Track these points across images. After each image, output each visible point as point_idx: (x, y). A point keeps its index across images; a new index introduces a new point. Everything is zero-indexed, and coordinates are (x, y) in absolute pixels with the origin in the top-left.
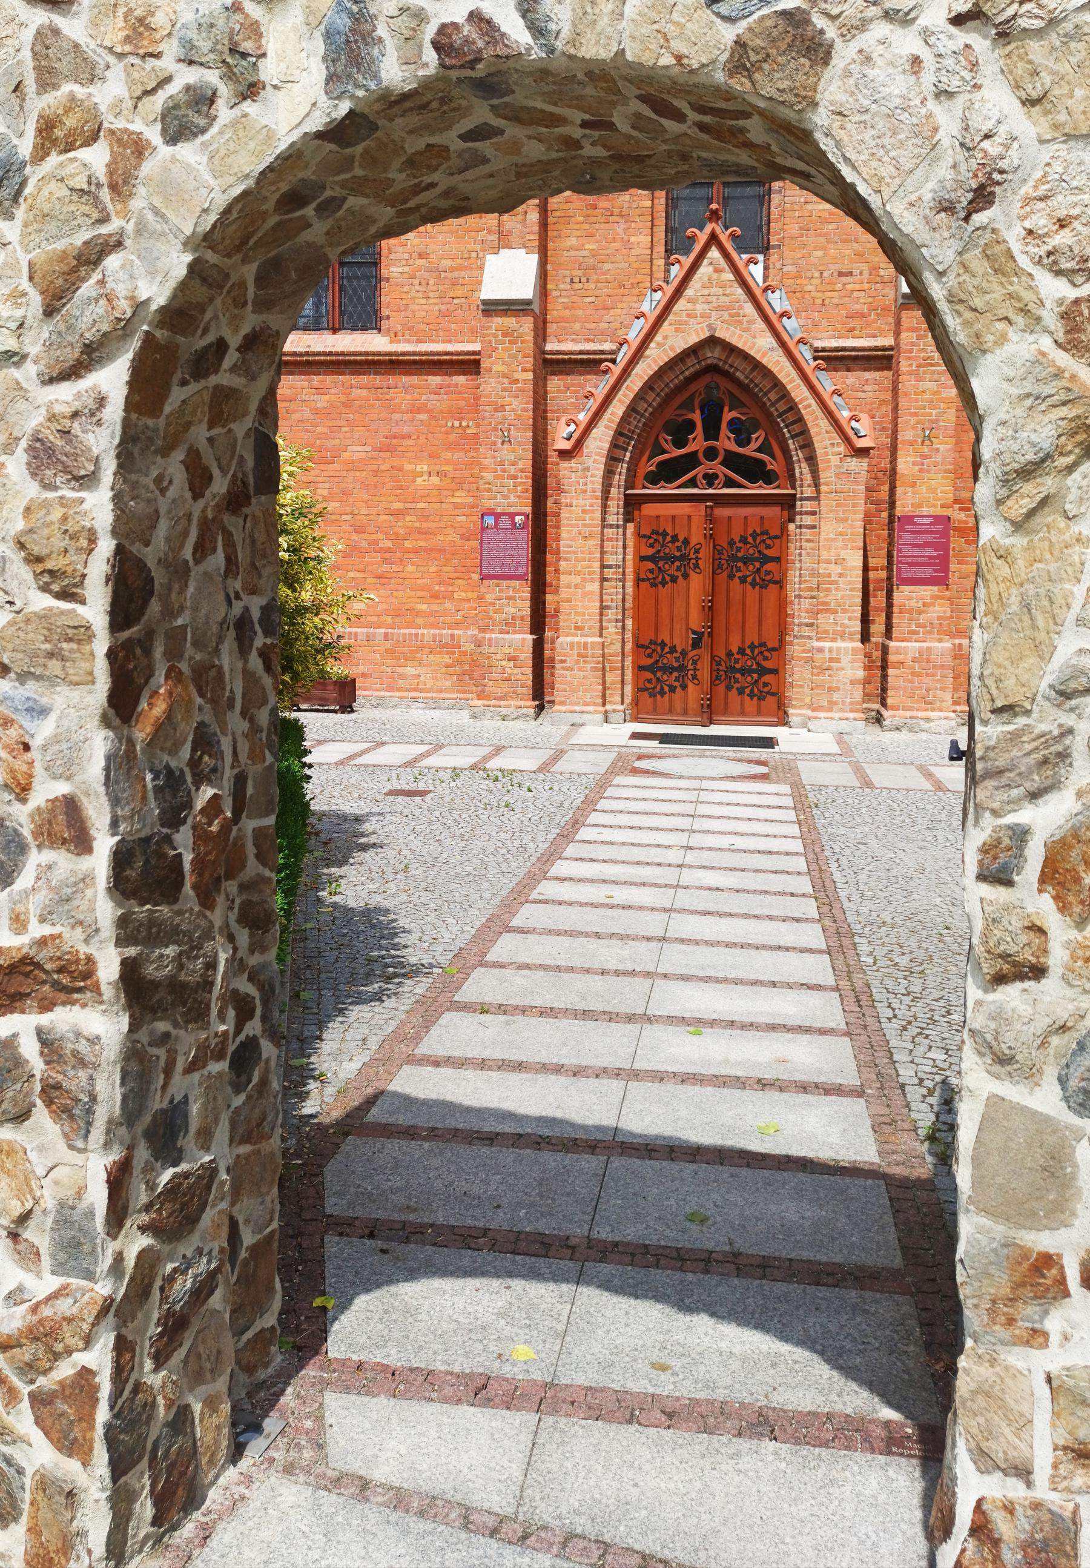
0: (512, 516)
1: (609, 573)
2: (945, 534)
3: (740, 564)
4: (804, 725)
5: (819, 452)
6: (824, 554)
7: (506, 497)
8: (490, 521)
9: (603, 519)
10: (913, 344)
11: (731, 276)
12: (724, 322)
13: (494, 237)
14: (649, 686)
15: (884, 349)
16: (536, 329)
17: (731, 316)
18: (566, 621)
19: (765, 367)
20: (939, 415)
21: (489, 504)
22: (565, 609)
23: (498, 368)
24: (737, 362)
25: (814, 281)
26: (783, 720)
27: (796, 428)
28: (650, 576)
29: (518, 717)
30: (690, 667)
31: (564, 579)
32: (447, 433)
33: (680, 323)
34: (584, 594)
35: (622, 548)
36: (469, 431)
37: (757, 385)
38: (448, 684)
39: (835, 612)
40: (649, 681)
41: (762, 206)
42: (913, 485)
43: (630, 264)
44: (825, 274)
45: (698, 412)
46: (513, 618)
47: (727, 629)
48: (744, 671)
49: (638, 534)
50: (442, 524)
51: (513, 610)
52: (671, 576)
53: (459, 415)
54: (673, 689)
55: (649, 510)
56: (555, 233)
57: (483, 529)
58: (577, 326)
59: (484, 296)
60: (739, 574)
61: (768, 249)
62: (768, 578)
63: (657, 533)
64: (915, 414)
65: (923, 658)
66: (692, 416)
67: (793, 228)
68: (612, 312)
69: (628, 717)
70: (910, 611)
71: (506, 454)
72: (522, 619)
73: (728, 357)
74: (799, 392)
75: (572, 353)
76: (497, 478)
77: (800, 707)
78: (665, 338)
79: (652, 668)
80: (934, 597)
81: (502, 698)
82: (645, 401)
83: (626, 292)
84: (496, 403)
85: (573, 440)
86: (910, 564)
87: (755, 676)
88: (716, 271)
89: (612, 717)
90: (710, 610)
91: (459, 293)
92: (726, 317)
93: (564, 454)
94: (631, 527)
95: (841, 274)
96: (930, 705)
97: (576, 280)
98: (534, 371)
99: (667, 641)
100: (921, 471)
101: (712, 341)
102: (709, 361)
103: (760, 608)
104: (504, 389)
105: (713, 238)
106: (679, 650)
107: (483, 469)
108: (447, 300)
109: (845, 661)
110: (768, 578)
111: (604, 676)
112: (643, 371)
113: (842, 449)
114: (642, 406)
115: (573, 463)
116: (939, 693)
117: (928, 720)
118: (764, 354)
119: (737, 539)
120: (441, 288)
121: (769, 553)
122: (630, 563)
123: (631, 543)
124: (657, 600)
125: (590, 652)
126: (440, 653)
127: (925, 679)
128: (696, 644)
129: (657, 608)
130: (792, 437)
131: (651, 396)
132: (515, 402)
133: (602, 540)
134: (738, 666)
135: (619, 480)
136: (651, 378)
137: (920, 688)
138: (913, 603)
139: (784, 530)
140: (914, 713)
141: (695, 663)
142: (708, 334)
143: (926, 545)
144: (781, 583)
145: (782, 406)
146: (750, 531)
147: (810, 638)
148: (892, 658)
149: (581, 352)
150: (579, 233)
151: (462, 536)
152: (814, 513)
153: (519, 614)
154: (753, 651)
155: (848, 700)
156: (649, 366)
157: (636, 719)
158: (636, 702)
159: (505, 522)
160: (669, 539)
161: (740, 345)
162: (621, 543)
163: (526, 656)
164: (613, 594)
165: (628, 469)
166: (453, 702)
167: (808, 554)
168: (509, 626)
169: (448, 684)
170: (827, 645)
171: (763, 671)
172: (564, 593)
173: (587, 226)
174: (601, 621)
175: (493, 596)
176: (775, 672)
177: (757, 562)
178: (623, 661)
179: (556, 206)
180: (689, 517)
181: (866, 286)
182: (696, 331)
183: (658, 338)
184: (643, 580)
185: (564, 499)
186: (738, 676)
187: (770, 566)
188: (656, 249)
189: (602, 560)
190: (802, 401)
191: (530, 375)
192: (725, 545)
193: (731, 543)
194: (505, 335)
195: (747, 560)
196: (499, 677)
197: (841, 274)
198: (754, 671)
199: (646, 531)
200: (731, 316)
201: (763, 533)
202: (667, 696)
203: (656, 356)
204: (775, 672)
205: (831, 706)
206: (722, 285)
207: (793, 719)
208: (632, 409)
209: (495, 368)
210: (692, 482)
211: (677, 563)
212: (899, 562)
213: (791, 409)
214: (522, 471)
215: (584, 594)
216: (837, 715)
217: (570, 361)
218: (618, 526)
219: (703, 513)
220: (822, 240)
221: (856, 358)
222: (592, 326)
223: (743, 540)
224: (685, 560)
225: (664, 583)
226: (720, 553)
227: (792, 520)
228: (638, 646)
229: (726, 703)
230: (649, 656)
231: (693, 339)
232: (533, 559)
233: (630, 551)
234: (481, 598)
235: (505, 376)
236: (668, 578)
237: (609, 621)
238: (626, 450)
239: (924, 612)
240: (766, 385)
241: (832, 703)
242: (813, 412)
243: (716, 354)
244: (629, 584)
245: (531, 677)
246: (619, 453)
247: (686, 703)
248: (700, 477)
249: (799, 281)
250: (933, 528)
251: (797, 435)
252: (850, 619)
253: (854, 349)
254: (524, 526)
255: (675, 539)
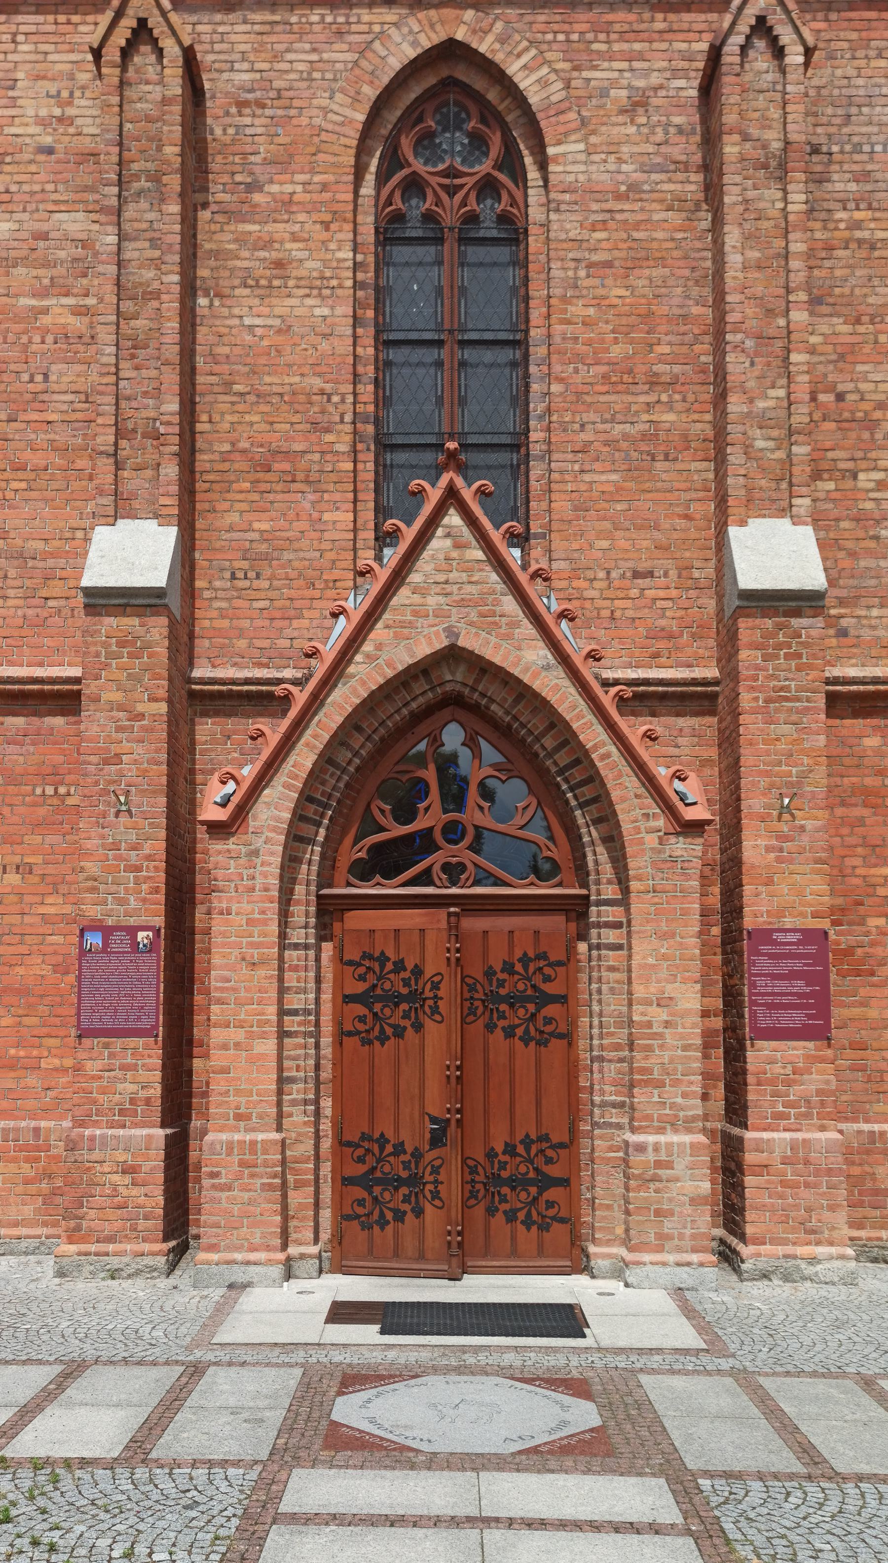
0: (132, 931)
1: (292, 1023)
2: (821, 958)
3: (503, 1007)
4: (618, 1273)
5: (626, 827)
6: (639, 991)
7: (122, 902)
8: (94, 940)
9: (283, 936)
10: (757, 668)
11: (480, 555)
12: (471, 624)
13: (108, 500)
14: (360, 1211)
15: (705, 682)
16: (173, 636)
17: (482, 615)
18: (219, 1105)
19: (536, 695)
20: (802, 776)
21: (93, 912)
22: (218, 1085)
23: (112, 695)
24: (493, 689)
25: (597, 584)
26: (579, 1263)
27: (587, 792)
28: (361, 1027)
29: (138, 1273)
30: (428, 1178)
31: (217, 1036)
32: (34, 805)
33: (403, 625)
34: (251, 1060)
35: (314, 982)
36: (70, 801)
37: (523, 725)
38: (28, 1211)
39: (660, 1084)
40: (361, 1202)
41: (516, 479)
42: (769, 882)
43: (322, 552)
44: (614, 574)
45: (432, 767)
46: (132, 1101)
47: (486, 1111)
48: (514, 1183)
49: (340, 959)
50: (23, 949)
51: (133, 1088)
52: (395, 1027)
53: (55, 776)
54: (400, 1216)
55: (356, 920)
56: (207, 506)
57: (83, 953)
58: (242, 644)
59: (85, 582)
60: (502, 1023)
61: (527, 539)
62: (549, 1029)
63: (371, 957)
64: (767, 774)
65: (799, 1155)
66: (421, 773)
67: (562, 506)
68: (295, 623)
69: (326, 1265)
70: (773, 1082)
71: (123, 830)
72: (148, 1101)
73: (478, 681)
74: (592, 734)
75: (233, 682)
76: (108, 870)
77: (608, 1243)
78: (379, 647)
79: (366, 1181)
80: (812, 1060)
81: (110, 1239)
82: (349, 747)
83: (317, 594)
84: (108, 750)
85: (231, 806)
86: (771, 1006)
87: (533, 1190)
88: (457, 546)
89: (299, 1267)
90: (458, 1082)
91: (56, 592)
92: (473, 616)
93: (218, 829)
94: (328, 948)
95: (636, 575)
96: (813, 1235)
97: (240, 575)
98: (170, 702)
99: (390, 1134)
100: (779, 860)
101: (452, 654)
102: (448, 687)
103: (538, 1078)
104: (119, 729)
105: (452, 495)
106: (409, 1148)
107: (87, 855)
108: (36, 602)
109: (680, 1165)
110: (549, 1029)
111: (285, 1196)
112: (344, 699)
113: (661, 823)
114: (343, 756)
115: (231, 844)
116: (827, 1215)
117: (813, 1260)
118: (535, 675)
119: (498, 967)
120: (28, 583)
121: (550, 988)
122: (327, 1008)
123: (328, 975)
124: (372, 1067)
125: (261, 1158)
126: (15, 1160)
127: (803, 1192)
128: (437, 1140)
129: (372, 1082)
130: (581, 806)
131: (357, 741)
132: (139, 749)
133: (281, 969)
134: (505, 1174)
135: (308, 870)
136: (356, 709)
137: (796, 1207)
138: (778, 1069)
139: (571, 951)
140: (789, 1249)
141: (436, 1171)
142: (446, 643)
143: (792, 975)
144: (568, 1037)
145: (563, 759)
146: (518, 954)
147: (619, 1127)
148: (750, 1158)
149: (247, 681)
150: (244, 506)
151: (56, 968)
152: (617, 925)
153: (143, 1094)
154: (528, 1150)
155: (688, 1232)
156: (354, 691)
157: (341, 1262)
158: (338, 1239)
159: (119, 942)
160: (389, 966)
161: (497, 660)
162: (312, 974)
163: (154, 1163)
164: (300, 1062)
165: (323, 856)
166: (34, 1243)
167: (612, 990)
168: (125, 1114)
169: (28, 1211)
170: (651, 1139)
171: (546, 1182)
172: (218, 1059)
173: (256, 497)
174: (279, 1104)
175: (98, 1064)
176: (565, 1182)
177: (530, 1007)
178: (317, 1169)
179: (208, 466)
180: (422, 931)
181: (674, 593)
182: (428, 638)
183: (368, 647)
184: (350, 1034)
185: (219, 902)
186: (506, 1190)
187: (551, 1010)
188: (361, 535)
189: (280, 1001)
190: (596, 747)
191: (163, 708)
192: (480, 977)
193: (489, 973)
194: (121, 644)
195: (513, 1001)
196: (108, 1202)
197: (636, 575)
198: (532, 1182)
199: (352, 954)
200: (482, 615)
201: (538, 957)
202: (389, 1229)
203: (365, 676)
204: (565, 1182)
205: (661, 1243)
206: (468, 567)
207: (599, 1264)
208: (326, 760)
209: (104, 696)
210: (425, 878)
211: (404, 1006)
212: (753, 1003)
213: (577, 762)
214: (149, 858)
215: (251, 1060)
216: (671, 1258)
217: (230, 695)
218: (306, 947)
219: (444, 925)
220: (607, 525)
221: (664, 696)
222: (266, 643)
223: (508, 967)
224: (416, 1000)
225: (383, 1039)
226: (472, 989)
227: (583, 936)
228: (341, 1143)
229: (487, 1236)
230: (361, 1160)
231: (424, 649)
232: (168, 1000)
233: (327, 986)
234: (78, 1068)
235: (121, 708)
236: (389, 1031)
237: (294, 1103)
238: (319, 824)
239: (795, 1082)
240: (537, 724)
241: (663, 1237)
242: (615, 765)
243: (459, 677)
244: (326, 1041)
245: (161, 1200)
246: (307, 830)
247: (422, 1240)
248: (437, 868)
249: (575, 583)
250: (801, 950)
251: (588, 803)
252: (684, 1095)
253: (661, 682)
254: (152, 948)
255: (400, 966)
